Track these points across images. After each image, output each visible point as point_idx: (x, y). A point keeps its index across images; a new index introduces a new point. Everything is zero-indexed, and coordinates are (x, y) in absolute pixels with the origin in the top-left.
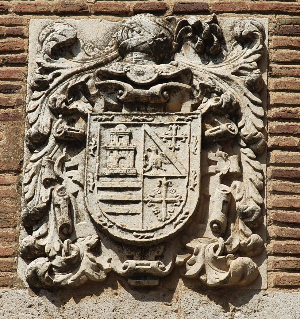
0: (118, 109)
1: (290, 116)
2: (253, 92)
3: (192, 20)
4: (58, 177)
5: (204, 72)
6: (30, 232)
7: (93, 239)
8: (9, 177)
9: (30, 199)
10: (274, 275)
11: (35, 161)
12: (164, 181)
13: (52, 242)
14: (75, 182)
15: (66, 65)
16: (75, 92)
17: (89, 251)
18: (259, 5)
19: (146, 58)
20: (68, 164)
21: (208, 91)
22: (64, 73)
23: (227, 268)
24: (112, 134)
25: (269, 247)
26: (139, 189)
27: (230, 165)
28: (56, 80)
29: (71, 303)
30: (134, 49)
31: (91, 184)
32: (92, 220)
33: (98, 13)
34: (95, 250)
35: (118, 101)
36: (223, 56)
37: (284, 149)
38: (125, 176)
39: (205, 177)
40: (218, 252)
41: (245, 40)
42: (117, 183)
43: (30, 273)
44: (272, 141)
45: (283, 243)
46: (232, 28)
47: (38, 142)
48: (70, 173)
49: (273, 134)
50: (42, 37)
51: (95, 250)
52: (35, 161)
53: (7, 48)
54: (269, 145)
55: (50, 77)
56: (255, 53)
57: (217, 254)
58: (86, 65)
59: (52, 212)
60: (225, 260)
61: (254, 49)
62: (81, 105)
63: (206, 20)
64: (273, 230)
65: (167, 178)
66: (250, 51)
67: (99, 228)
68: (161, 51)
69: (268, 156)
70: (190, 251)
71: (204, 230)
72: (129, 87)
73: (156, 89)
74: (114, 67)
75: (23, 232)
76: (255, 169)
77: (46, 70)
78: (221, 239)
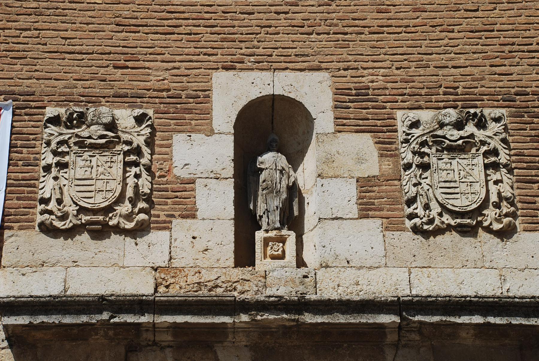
0: (442, 151)
1: (521, 154)
2: (503, 143)
3: (472, 111)
4: (419, 182)
5: (480, 134)
6: (409, 207)
7: (439, 210)
8: (396, 182)
9: (408, 192)
10: (522, 225)
11: (408, 175)
12: (469, 184)
13: (420, 211)
14: (427, 184)
15: (417, 132)
16: (423, 144)
17: (438, 215)
18: (500, 104)
19: (453, 128)
20: (423, 176)
21: (483, 143)
22: (416, 135)
23: (502, 223)
24: (443, 163)
25: (519, 213)
26: (458, 187)
27: (496, 176)
28: (413, 139)
29: (432, 238)
30: (447, 125)
31: (436, 185)
32: (438, 201)
33: (427, 108)
34: (440, 215)
35: (442, 148)
36: (487, 127)
37: (519, 169)
38: (451, 182)
39: (487, 181)
40: (497, 215)
41: (497, 120)
42: (447, 185)
43: (412, 225)
44: (514, 165)
45: (525, 211)
46: (490, 114)
47: (408, 166)
48: (425, 180)
49: (514, 162)
50: (403, 120)
51: (440, 215)
52: (408, 175)
53: (388, 124)
54: (513, 167)
55: (410, 137)
56: (502, 125)
57: (497, 216)
58: (425, 132)
59: (418, 198)
60: (501, 219)
61: (501, 124)
62: (426, 150)
63: (478, 111)
64: (519, 205)
65: (470, 182)
66: (499, 125)
67: (441, 205)
68: (459, 125)
69: (513, 172)
70: (484, 215)
71: (489, 205)
72: (447, 142)
73: (460, 142)
74: (439, 133)
75: (406, 207)
76: (508, 178)
77: (408, 134)
78: (497, 210)
